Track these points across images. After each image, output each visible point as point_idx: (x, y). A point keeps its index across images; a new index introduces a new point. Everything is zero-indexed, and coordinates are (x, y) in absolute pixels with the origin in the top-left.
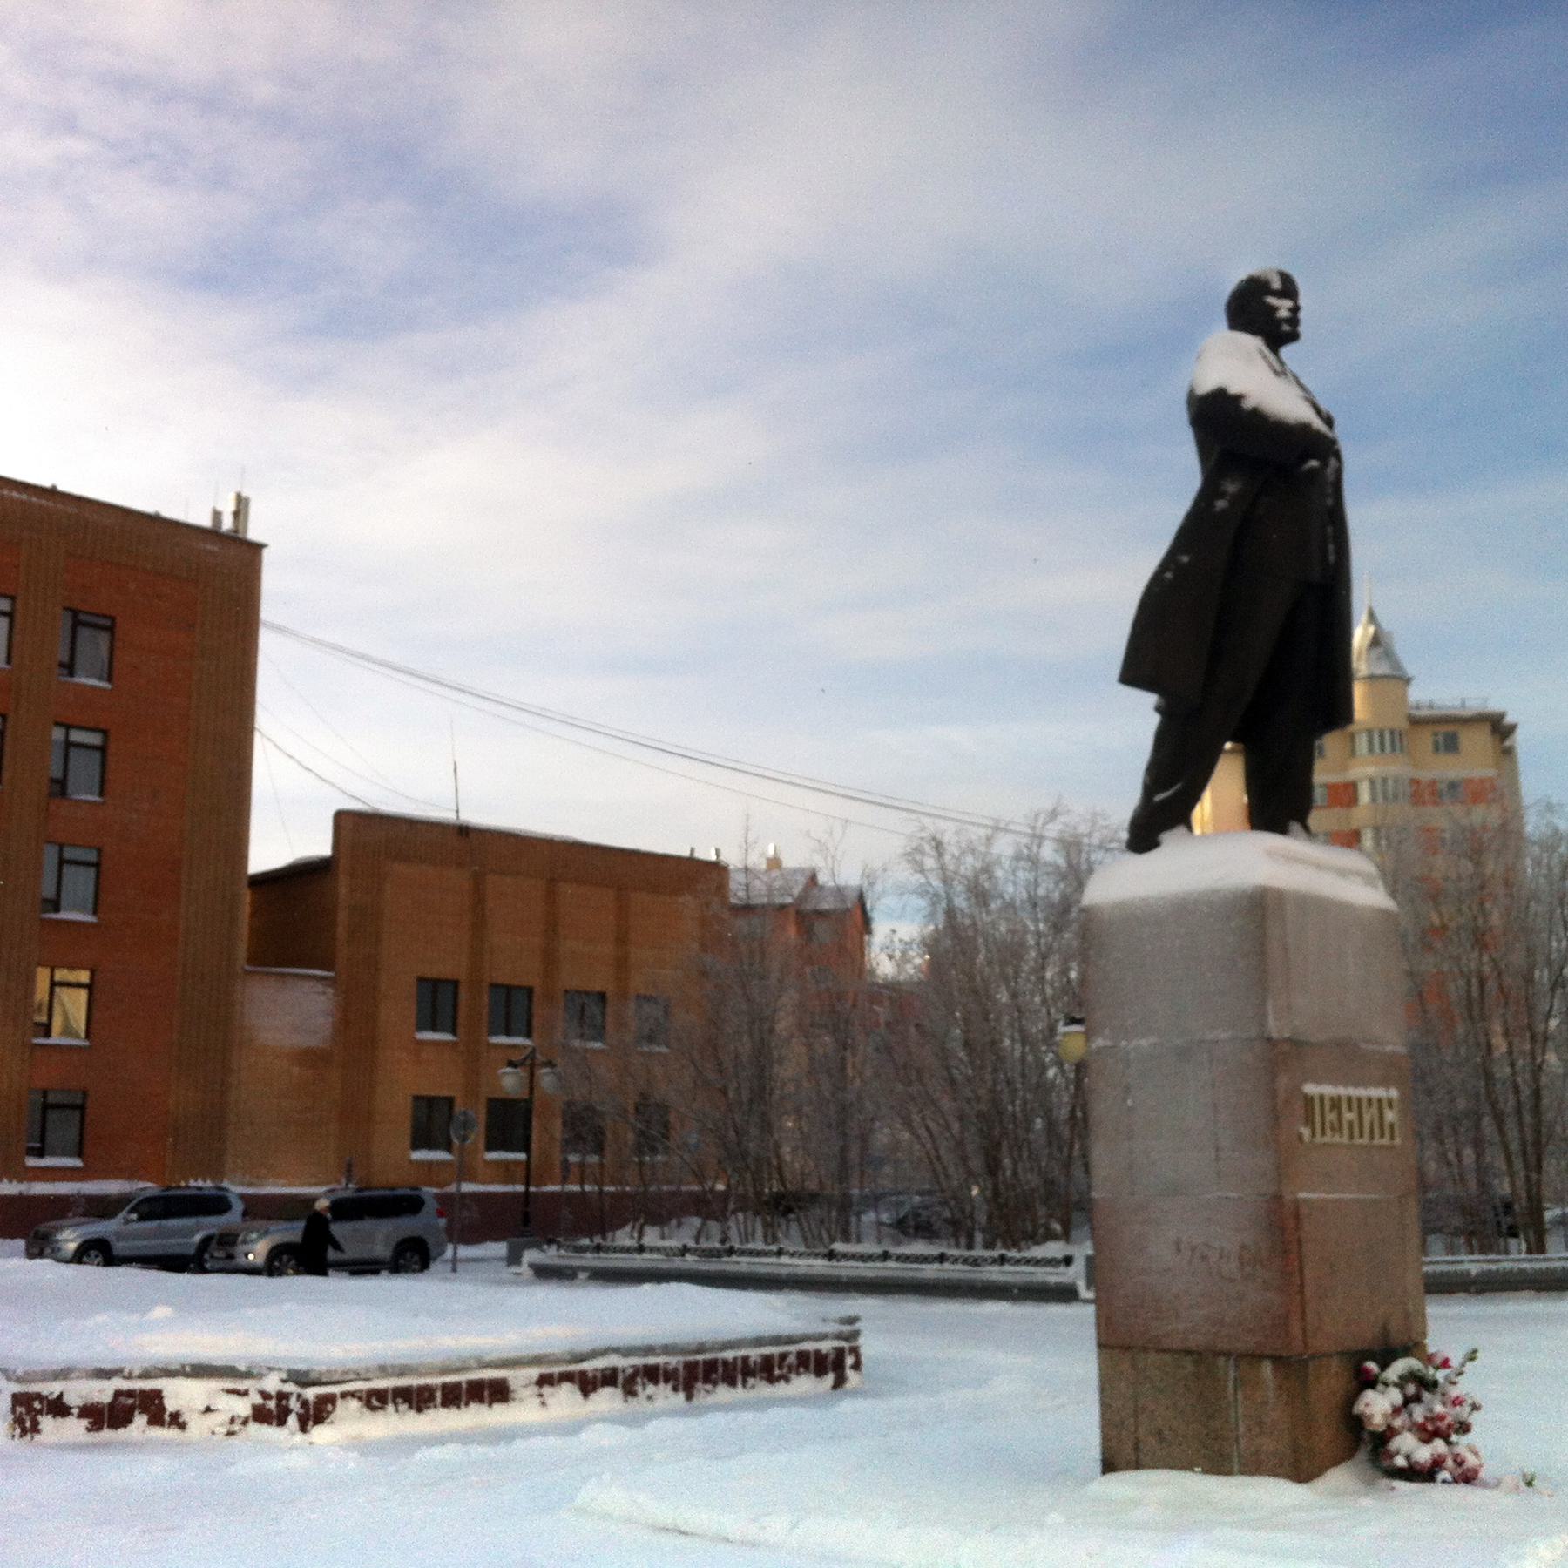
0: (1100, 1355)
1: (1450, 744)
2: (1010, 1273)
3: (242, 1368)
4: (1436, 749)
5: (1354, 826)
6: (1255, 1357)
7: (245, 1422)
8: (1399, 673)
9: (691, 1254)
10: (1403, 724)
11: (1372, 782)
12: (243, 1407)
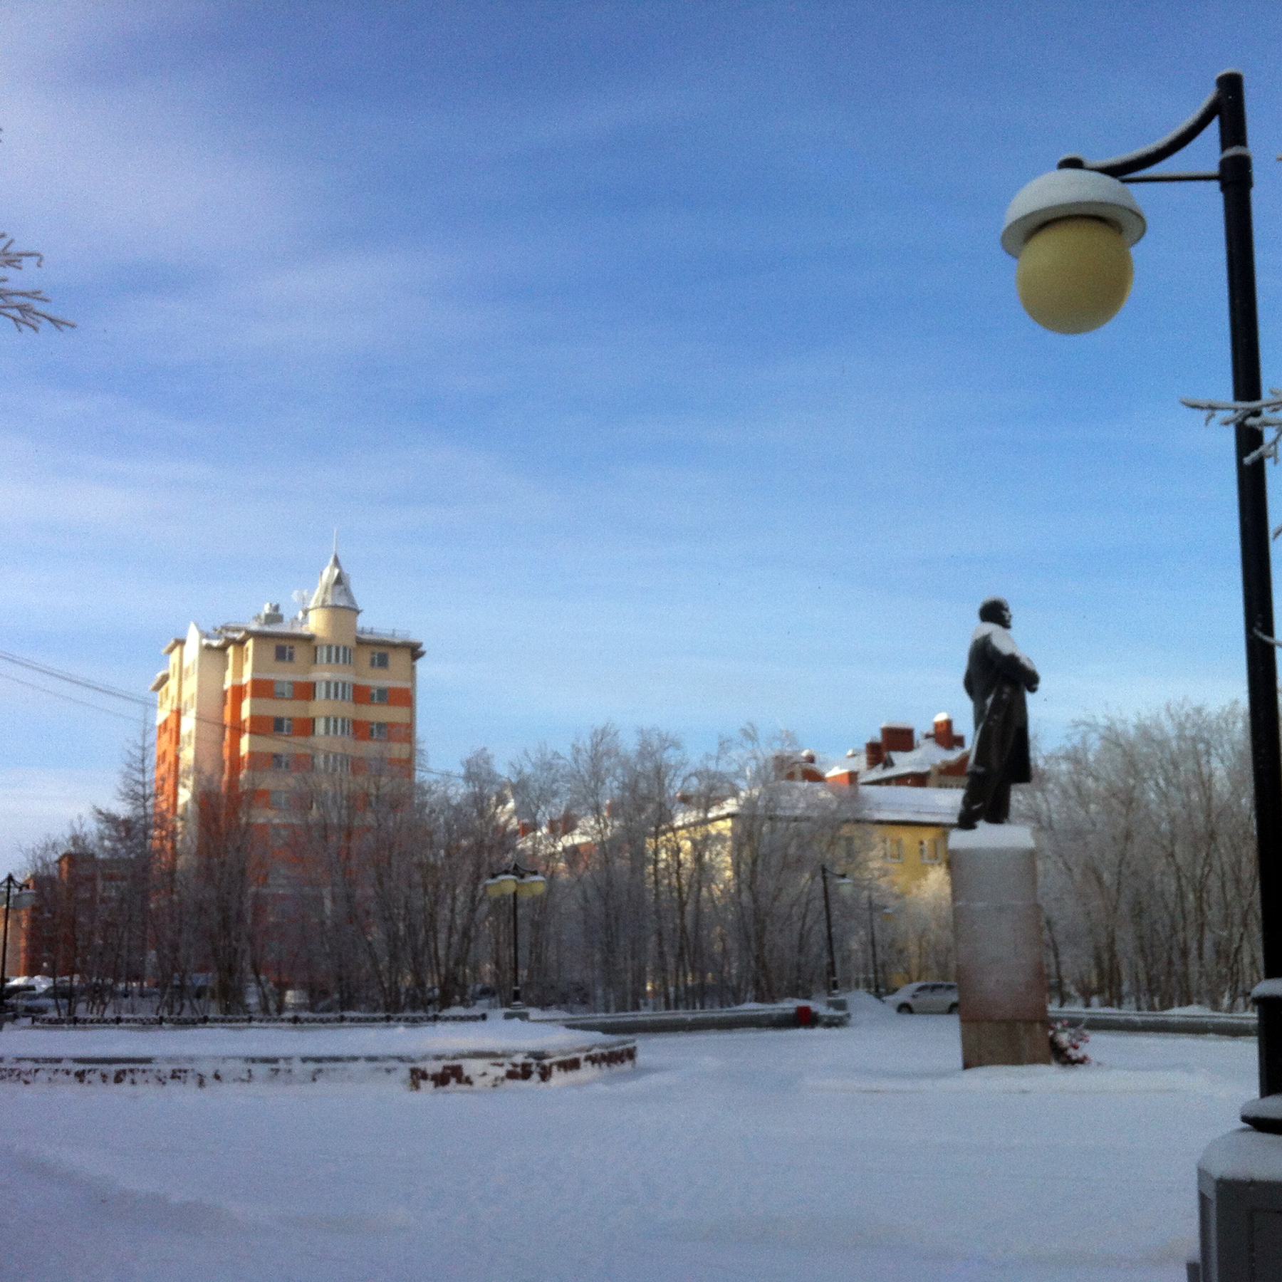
1: (382, 662)
2: (631, 1016)
3: (499, 1052)
4: (372, 664)
5: (311, 715)
6: (1032, 1022)
7: (502, 1079)
8: (354, 607)
10: (351, 643)
12: (501, 1072)
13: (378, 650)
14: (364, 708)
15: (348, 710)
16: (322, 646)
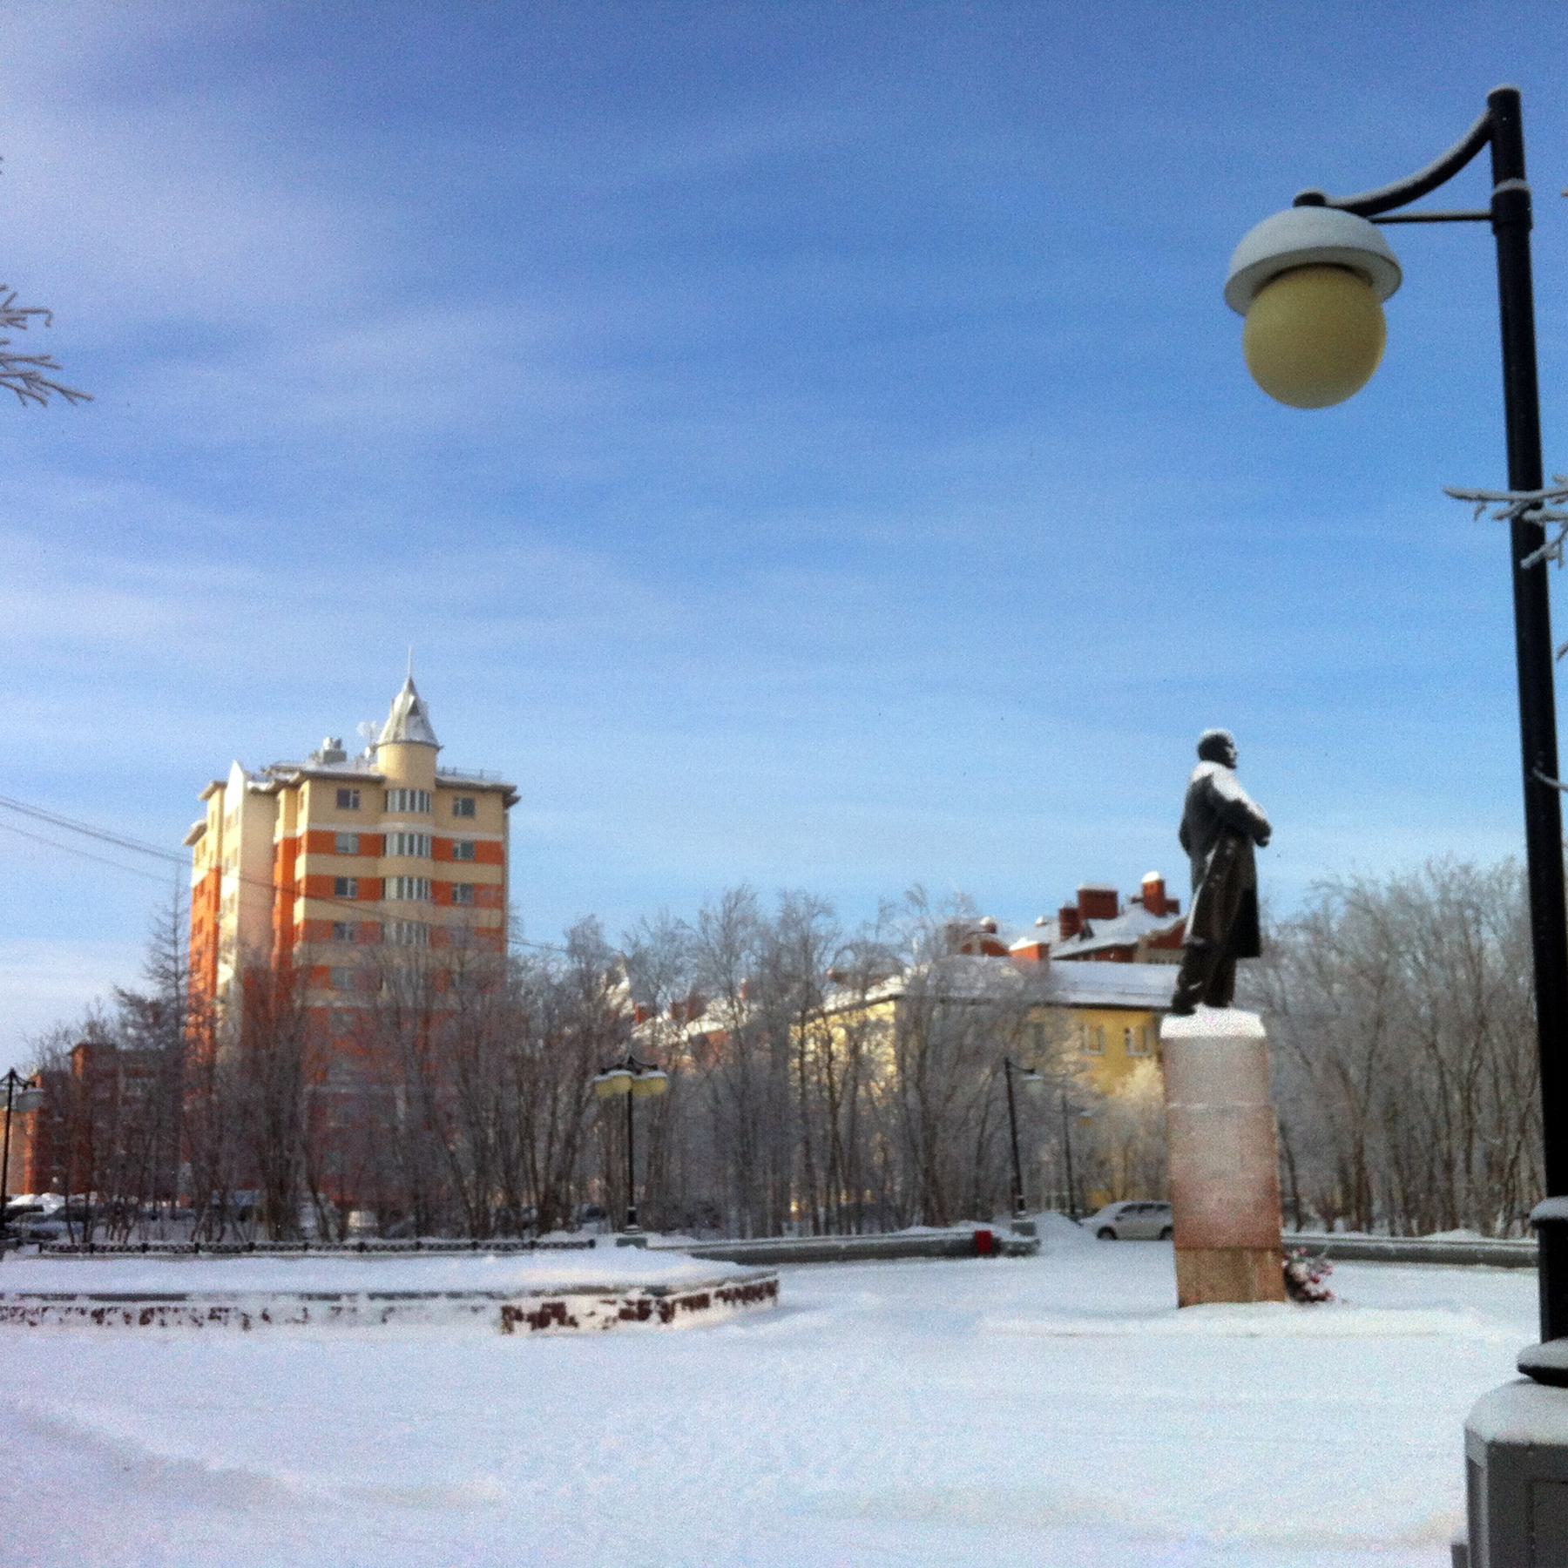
0: (1176, 1256)
1: (468, 809)
3: (611, 1287)
4: (455, 812)
5: (381, 874)
7: (615, 1320)
8: (433, 742)
9: (204, 1251)
10: (429, 786)
11: (401, 836)
12: (613, 1311)
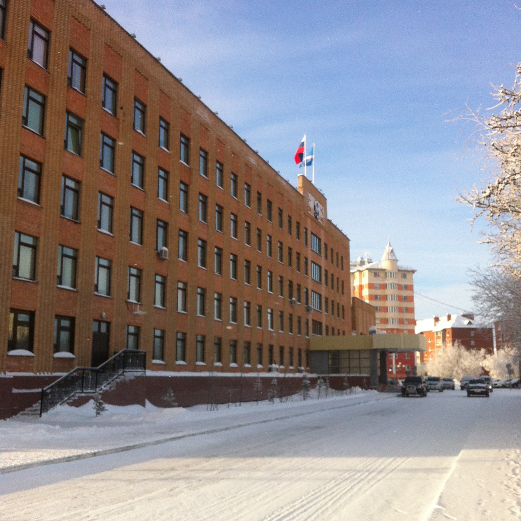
1: (405, 276)
13: (404, 273)
14: (401, 291)
15: (396, 292)
16: (388, 272)
